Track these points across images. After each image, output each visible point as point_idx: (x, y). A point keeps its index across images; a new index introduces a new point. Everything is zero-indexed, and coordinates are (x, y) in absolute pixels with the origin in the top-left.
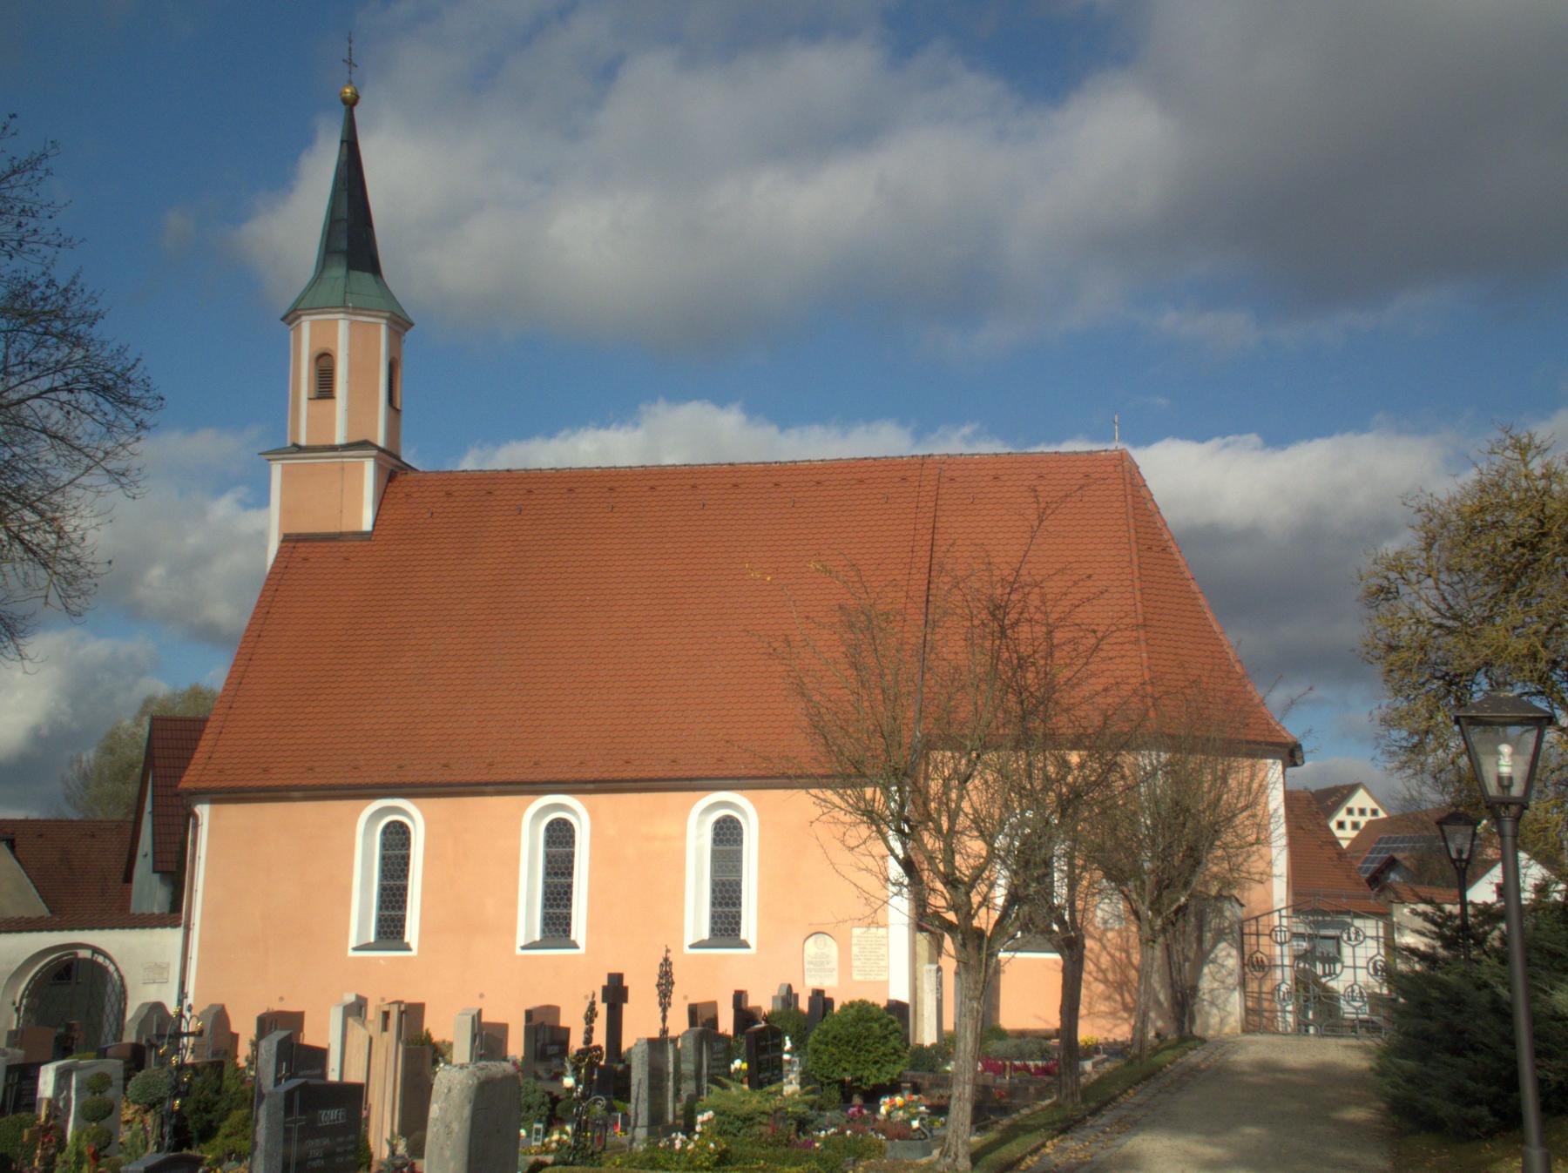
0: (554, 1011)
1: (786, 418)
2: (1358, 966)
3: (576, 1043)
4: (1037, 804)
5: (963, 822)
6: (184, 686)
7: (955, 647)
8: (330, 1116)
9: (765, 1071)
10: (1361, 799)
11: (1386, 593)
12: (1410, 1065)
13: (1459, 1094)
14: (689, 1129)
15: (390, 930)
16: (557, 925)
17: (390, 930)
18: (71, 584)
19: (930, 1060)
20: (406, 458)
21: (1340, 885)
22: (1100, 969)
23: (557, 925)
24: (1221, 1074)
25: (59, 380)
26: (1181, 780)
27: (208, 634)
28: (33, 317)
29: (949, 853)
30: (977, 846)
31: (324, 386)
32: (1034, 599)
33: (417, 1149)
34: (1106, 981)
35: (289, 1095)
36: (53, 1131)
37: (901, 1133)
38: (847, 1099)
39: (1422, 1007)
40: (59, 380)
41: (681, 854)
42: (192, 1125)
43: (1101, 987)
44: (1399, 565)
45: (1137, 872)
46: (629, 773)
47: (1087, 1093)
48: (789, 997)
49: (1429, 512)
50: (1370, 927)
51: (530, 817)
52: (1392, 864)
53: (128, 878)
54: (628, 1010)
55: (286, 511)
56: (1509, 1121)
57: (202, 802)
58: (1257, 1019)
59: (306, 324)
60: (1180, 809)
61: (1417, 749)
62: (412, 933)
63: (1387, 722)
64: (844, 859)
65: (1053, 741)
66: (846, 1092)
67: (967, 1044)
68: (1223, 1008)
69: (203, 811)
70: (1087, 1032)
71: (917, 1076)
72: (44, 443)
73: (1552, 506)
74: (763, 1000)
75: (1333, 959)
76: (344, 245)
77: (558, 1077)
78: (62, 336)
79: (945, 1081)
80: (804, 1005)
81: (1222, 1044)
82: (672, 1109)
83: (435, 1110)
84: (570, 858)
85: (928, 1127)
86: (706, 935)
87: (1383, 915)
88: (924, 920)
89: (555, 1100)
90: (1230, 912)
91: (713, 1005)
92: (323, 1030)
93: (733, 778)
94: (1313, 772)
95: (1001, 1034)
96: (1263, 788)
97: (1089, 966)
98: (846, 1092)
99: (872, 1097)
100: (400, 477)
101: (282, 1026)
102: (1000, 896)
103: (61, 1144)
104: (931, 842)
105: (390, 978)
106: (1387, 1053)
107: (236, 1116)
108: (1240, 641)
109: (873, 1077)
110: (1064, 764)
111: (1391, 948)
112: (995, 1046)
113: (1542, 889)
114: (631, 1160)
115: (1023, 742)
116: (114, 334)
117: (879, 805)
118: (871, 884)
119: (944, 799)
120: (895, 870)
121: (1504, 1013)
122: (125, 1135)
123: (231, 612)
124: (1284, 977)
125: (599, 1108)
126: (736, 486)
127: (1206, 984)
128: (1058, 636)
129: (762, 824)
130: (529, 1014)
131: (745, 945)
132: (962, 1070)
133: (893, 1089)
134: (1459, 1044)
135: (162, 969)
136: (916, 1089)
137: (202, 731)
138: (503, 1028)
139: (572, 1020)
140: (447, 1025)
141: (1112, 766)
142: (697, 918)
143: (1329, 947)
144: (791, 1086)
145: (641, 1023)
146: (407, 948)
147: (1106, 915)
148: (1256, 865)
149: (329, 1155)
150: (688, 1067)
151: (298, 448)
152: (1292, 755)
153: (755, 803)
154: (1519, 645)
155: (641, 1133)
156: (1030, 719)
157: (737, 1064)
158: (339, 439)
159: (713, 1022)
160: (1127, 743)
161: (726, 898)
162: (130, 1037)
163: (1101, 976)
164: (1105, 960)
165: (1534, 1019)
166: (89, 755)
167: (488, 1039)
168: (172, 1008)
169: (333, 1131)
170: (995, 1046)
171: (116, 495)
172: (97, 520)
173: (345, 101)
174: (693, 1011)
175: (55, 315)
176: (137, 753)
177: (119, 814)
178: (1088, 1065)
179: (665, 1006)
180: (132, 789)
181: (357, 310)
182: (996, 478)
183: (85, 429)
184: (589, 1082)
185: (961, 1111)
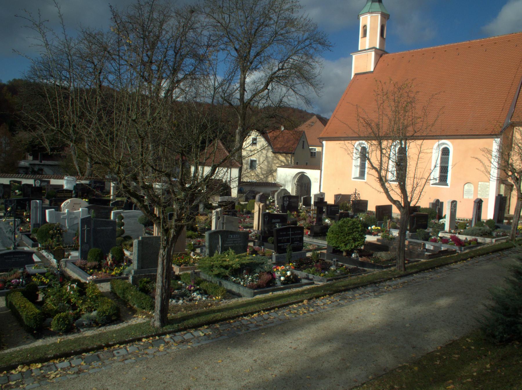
31: (365, 35)
84: (448, 159)
86: (358, 176)
93: (446, 136)
126: (469, 47)
129: (454, 148)
131: (447, 185)
146: (447, 185)
153: (452, 143)
158: (367, 48)
161: (444, 170)
181: (372, 13)
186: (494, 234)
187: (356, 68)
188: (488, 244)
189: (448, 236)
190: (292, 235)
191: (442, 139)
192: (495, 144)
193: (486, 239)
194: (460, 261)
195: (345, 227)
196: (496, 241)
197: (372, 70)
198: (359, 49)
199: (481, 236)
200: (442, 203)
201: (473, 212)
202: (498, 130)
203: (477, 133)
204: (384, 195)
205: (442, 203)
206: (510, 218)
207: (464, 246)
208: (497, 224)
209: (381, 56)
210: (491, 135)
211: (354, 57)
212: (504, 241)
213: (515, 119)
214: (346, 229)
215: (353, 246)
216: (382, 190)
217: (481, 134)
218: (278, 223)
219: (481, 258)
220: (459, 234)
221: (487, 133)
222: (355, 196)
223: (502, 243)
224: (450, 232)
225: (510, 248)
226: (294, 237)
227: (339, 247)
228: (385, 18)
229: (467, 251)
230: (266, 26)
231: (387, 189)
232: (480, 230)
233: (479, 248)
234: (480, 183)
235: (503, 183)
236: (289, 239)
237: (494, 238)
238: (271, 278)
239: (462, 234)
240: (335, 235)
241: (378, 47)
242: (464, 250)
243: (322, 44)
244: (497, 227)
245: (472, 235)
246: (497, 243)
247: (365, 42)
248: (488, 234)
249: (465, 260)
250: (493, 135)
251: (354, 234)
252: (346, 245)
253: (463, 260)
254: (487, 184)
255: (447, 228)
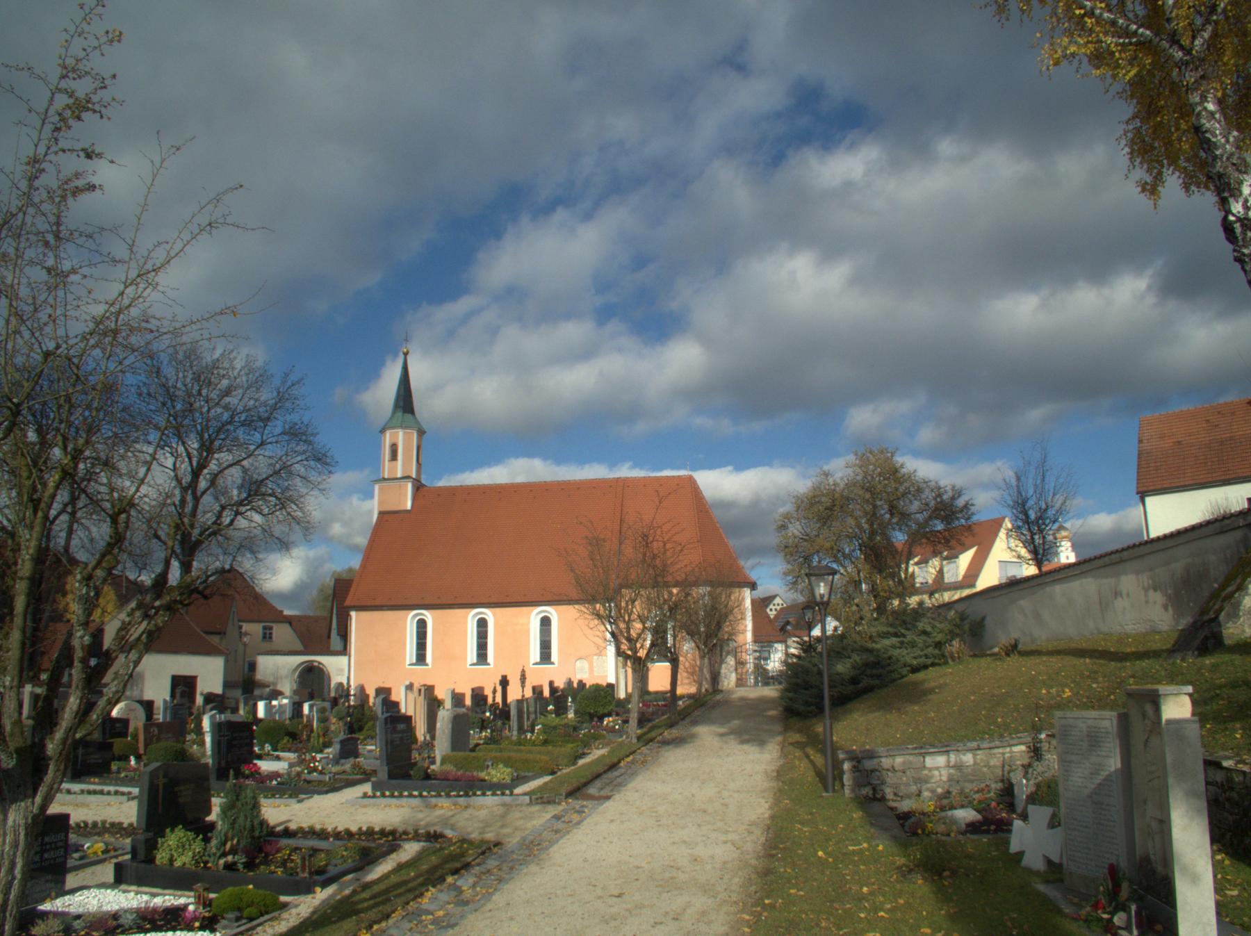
0: (482, 689)
1: (559, 460)
2: (775, 662)
3: (490, 700)
4: (661, 608)
5: (634, 616)
6: (346, 567)
7: (628, 551)
8: (401, 726)
9: (561, 709)
10: (778, 600)
11: (783, 527)
12: (790, 695)
13: (807, 703)
14: (532, 731)
15: (421, 658)
16: (482, 656)
17: (421, 658)
18: (308, 529)
19: (622, 704)
20: (423, 482)
21: (768, 633)
23: (482, 656)
24: (726, 702)
25: (304, 457)
26: (714, 598)
27: (354, 548)
28: (295, 435)
29: (628, 629)
30: (638, 626)
32: (659, 532)
33: (433, 737)
35: (386, 719)
36: (309, 726)
37: (612, 730)
38: (591, 719)
39: (796, 675)
40: (304, 457)
41: (528, 631)
42: (355, 726)
44: (787, 516)
45: (699, 633)
46: (508, 600)
47: (680, 713)
48: (570, 682)
49: (797, 497)
50: (780, 647)
51: (471, 618)
52: (788, 623)
53: (329, 637)
54: (509, 688)
55: (380, 503)
56: (821, 710)
58: (741, 682)
59: (388, 434)
60: (714, 608)
61: (795, 583)
62: (429, 659)
63: (786, 574)
64: (589, 632)
65: (667, 585)
66: (591, 716)
67: (635, 699)
68: (729, 679)
69: (353, 614)
70: (680, 691)
71: (618, 710)
72: (298, 479)
73: (837, 495)
74: (560, 684)
75: (769, 658)
76: (401, 404)
77: (484, 712)
78: (305, 441)
79: (628, 711)
80: (575, 685)
81: (729, 692)
82: (526, 724)
83: (438, 725)
84: (486, 632)
85: (622, 727)
86: (538, 660)
87: (784, 641)
88: (619, 653)
89: (483, 721)
90: (732, 645)
91: (541, 686)
92: (399, 695)
94: (761, 592)
95: (649, 693)
96: (743, 599)
97: (681, 666)
98: (591, 716)
99: (601, 718)
101: (384, 692)
102: (648, 643)
103: (312, 731)
104: (622, 625)
105: (421, 676)
106: (786, 690)
107: (370, 724)
108: (732, 543)
109: (601, 711)
110: (671, 593)
111: (787, 654)
112: (647, 697)
113: (836, 629)
114: (511, 742)
115: (655, 585)
116: (323, 440)
117: (602, 612)
118: (600, 641)
119: (626, 610)
120: (609, 636)
121: (820, 673)
122: (333, 728)
123: (362, 540)
124: (750, 667)
125: (499, 723)
127: (723, 671)
128: (668, 546)
129: (559, 618)
130: (473, 690)
132: (634, 706)
133: (609, 715)
134: (807, 686)
135: (342, 670)
136: (617, 714)
137: (350, 587)
138: (463, 695)
139: (488, 692)
140: (442, 693)
141: (688, 595)
142: (535, 654)
143: (766, 655)
144: (571, 715)
145: (514, 694)
147: (687, 648)
148: (741, 627)
149: (402, 739)
150: (532, 709)
151: (384, 479)
152: (753, 586)
154: (827, 545)
155: (515, 733)
156: (658, 577)
157: (551, 707)
158: (399, 475)
159: (541, 692)
160: (696, 584)
162: (333, 694)
164: (687, 664)
165: (830, 676)
166: (315, 593)
167: (458, 699)
168: (345, 682)
169: (402, 732)
170: (647, 697)
171: (322, 498)
172: (315, 505)
174: (534, 688)
175: (303, 434)
176: (331, 592)
177: (325, 614)
178: (680, 703)
179: (523, 687)
180: (329, 604)
181: (406, 428)
183: (313, 476)
184: (495, 715)
185: (633, 722)
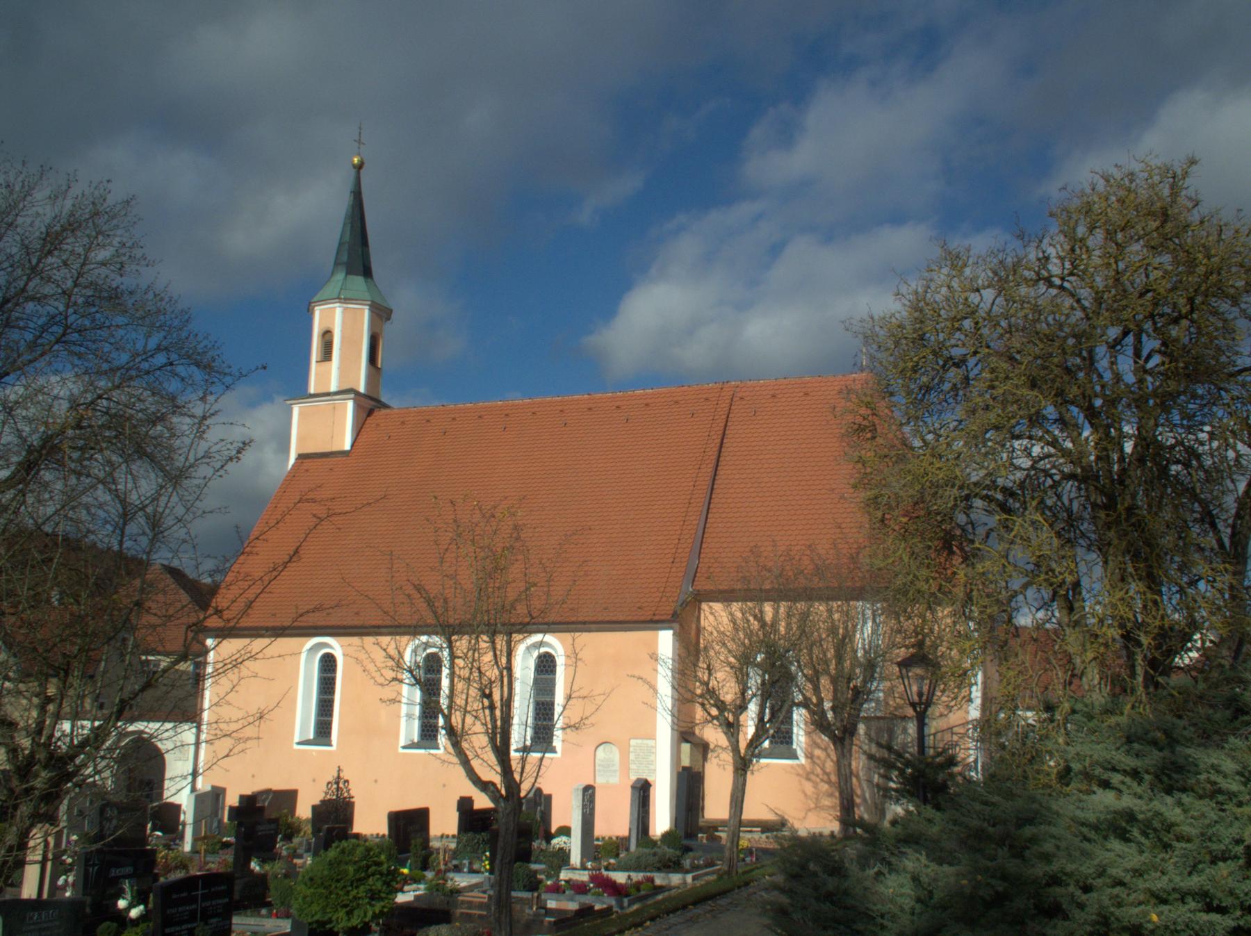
15: (323, 731)
17: (323, 731)
22: (825, 772)
31: (327, 354)
34: (829, 782)
43: (826, 786)
57: (211, 637)
76: (345, 258)
100: (376, 413)
158: (333, 388)
163: (825, 778)
173: (354, 166)
181: (347, 300)
182: (774, 396)
186: (687, 863)
187: (301, 439)
188: (678, 888)
189: (584, 877)
190: (205, 898)
191: (531, 632)
192: (665, 641)
193: (671, 875)
194: (629, 929)
195: (347, 864)
196: (694, 879)
197: (347, 447)
198: (312, 390)
199: (659, 870)
200: (549, 797)
201: (631, 814)
202: (668, 609)
203: (621, 618)
204: (460, 771)
205: (549, 797)
206: (713, 827)
207: (627, 895)
208: (685, 842)
209: (370, 413)
210: (651, 621)
211: (296, 410)
212: (714, 877)
213: (703, 585)
214: (351, 869)
215: (370, 914)
216: (455, 760)
217: (629, 618)
218: (125, 877)
219: (673, 919)
220: (607, 869)
221: (642, 618)
222: (338, 789)
223: (708, 883)
224: (584, 868)
225: (729, 891)
226: (208, 904)
227: (330, 921)
228: (380, 316)
229: (635, 907)
230: (32, 298)
231: (466, 756)
232: (655, 854)
233: (660, 897)
234: (633, 742)
235: (687, 741)
236: (196, 910)
237: (687, 872)
238: (803, 711)
239: (615, 870)
240: (322, 890)
241: (362, 389)
242: (629, 905)
243: (207, 367)
244: (687, 849)
245: (637, 869)
246: (698, 883)
247: (329, 373)
248: (672, 865)
249: (640, 924)
250: (657, 622)
251: (370, 881)
252: (350, 913)
253: (636, 925)
254: (650, 742)
255: (575, 858)
